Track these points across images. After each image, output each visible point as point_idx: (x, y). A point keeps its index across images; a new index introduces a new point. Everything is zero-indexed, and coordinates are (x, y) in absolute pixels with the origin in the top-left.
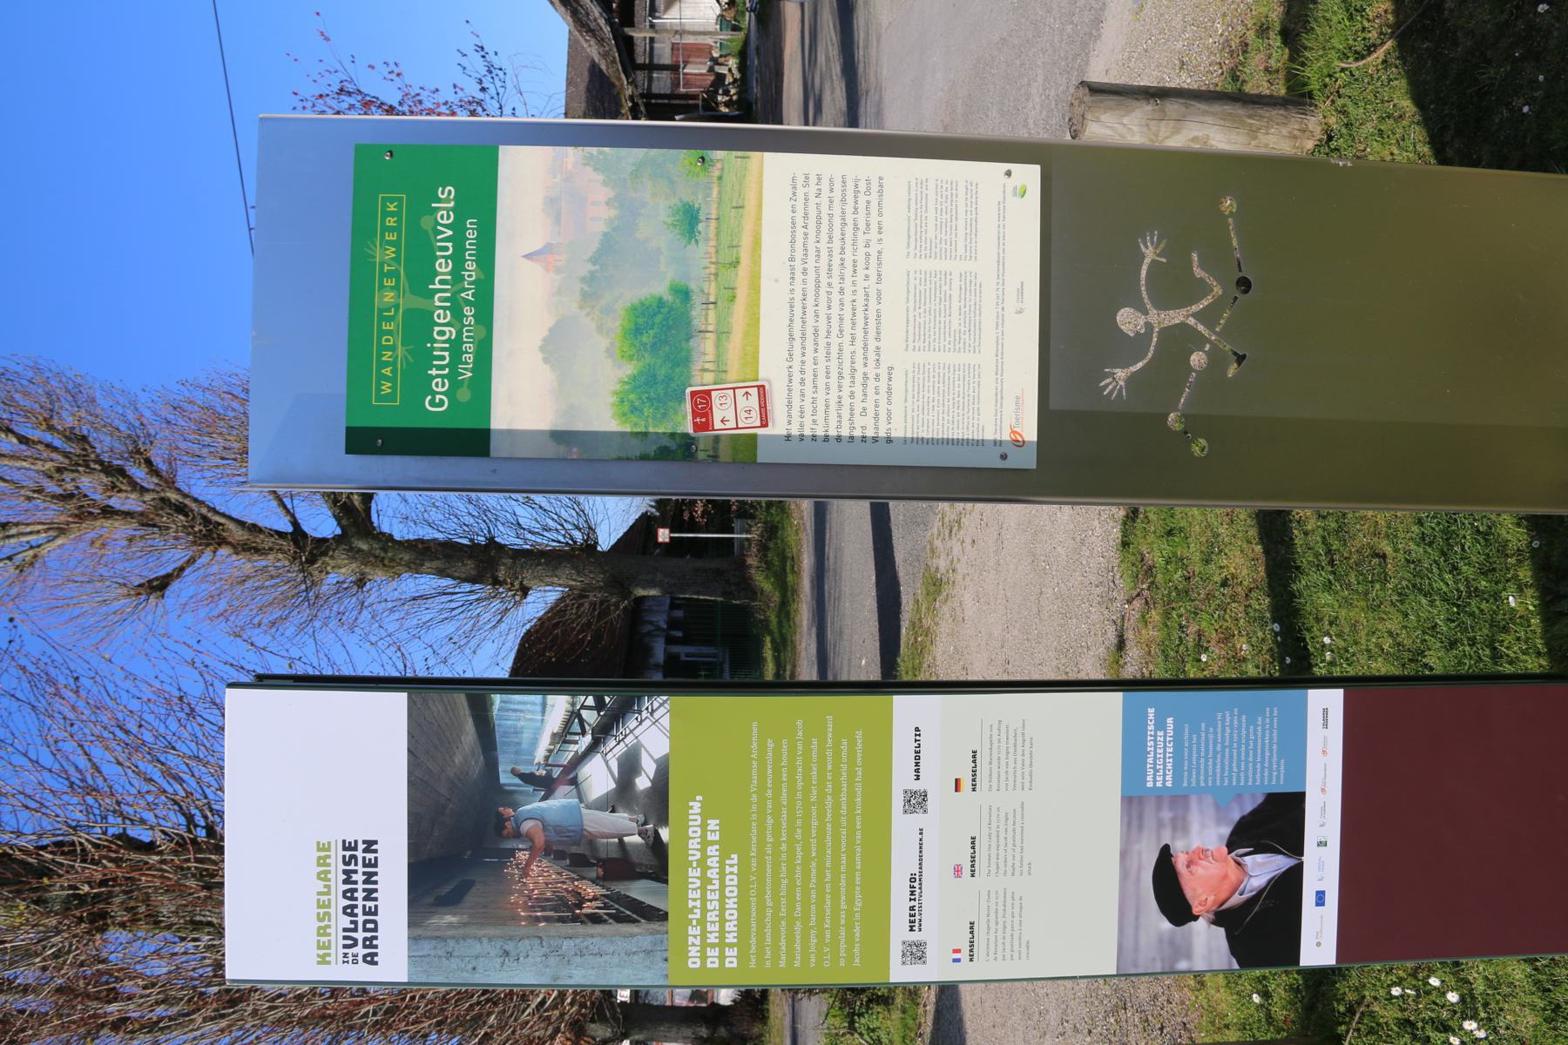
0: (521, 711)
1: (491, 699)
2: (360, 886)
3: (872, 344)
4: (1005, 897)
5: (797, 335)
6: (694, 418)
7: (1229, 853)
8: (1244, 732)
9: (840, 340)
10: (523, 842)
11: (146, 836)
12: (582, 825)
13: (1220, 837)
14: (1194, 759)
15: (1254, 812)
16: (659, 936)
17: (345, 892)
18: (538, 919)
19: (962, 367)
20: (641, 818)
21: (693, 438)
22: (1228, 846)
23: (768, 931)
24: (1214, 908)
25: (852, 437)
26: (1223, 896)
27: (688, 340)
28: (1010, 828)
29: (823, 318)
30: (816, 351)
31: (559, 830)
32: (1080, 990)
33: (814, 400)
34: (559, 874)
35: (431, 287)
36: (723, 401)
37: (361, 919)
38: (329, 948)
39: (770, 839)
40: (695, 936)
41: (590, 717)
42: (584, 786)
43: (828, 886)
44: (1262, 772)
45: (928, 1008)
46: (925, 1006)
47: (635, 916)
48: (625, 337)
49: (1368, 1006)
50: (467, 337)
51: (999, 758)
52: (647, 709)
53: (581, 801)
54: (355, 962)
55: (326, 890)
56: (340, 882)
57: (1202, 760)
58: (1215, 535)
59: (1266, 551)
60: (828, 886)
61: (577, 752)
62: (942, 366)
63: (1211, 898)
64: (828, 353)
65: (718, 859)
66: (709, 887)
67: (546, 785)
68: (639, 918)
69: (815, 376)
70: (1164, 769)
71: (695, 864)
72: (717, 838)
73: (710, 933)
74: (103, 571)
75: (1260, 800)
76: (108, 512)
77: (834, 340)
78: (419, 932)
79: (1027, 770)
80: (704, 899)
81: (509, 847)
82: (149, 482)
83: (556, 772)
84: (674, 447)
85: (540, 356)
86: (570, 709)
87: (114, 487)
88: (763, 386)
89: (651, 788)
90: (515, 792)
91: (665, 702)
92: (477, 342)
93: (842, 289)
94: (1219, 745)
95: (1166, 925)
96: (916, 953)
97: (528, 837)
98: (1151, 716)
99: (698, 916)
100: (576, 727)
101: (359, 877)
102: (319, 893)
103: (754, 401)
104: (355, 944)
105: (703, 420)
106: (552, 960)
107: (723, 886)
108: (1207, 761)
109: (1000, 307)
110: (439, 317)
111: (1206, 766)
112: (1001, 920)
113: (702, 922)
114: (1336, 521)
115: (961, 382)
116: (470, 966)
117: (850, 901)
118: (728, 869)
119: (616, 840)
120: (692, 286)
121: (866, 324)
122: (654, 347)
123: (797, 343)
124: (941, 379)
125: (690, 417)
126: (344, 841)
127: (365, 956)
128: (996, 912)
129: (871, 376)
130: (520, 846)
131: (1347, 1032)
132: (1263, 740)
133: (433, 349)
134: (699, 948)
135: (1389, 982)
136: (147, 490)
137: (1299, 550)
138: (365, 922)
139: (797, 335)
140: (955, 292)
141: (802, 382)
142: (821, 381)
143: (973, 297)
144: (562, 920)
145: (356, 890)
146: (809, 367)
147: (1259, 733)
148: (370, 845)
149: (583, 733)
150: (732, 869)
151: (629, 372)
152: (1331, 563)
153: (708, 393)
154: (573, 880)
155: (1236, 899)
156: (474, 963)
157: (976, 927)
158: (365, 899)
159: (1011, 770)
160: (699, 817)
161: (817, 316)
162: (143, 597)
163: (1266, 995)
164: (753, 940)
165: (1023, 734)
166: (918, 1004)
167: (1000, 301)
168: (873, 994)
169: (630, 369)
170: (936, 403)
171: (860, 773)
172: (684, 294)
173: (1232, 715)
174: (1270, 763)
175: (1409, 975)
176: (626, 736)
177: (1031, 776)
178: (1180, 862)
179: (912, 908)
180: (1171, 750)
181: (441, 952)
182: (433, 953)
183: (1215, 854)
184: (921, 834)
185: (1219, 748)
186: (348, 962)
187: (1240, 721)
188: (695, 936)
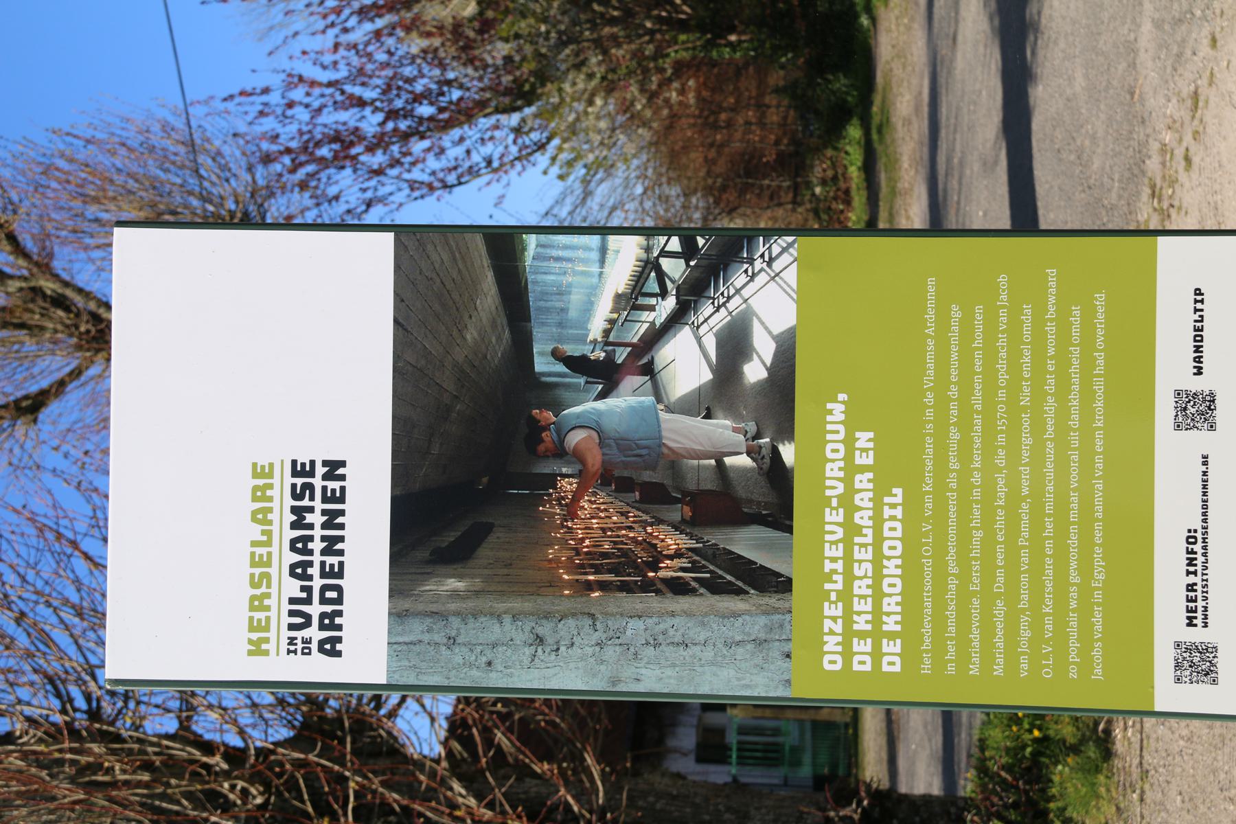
0: (569, 260)
1: (522, 241)
2: (318, 532)
10: (568, 463)
12: (660, 438)
16: (777, 617)
17: (293, 542)
18: (589, 586)
20: (752, 427)
23: (951, 613)
31: (624, 444)
34: (622, 514)
37: (317, 583)
38: (267, 629)
40: (834, 619)
41: (675, 269)
42: (664, 377)
43: (1049, 544)
47: (740, 584)
52: (762, 256)
53: (659, 400)
54: (307, 652)
56: (287, 525)
60: (1049, 544)
61: (653, 323)
65: (870, 494)
66: (857, 540)
71: (834, 502)
72: (870, 461)
73: (859, 613)
78: (406, 604)
80: (848, 559)
83: (621, 355)
86: (644, 256)
89: (767, 380)
91: (790, 245)
97: (577, 456)
99: (839, 586)
100: (652, 285)
101: (316, 519)
102: (255, 544)
104: (308, 624)
106: (611, 652)
107: (879, 539)
113: (846, 596)
116: (484, 659)
117: (1086, 570)
118: (887, 512)
126: (294, 462)
127: (322, 643)
130: (564, 470)
134: (839, 639)
138: (324, 589)
144: (626, 588)
145: (311, 539)
148: (334, 468)
149: (664, 294)
156: (489, 655)
158: (324, 552)
160: (841, 428)
164: (927, 629)
171: (1101, 362)
176: (729, 298)
179: (1191, 587)
182: (426, 638)
184: (1205, 463)
186: (295, 652)
188: (834, 619)
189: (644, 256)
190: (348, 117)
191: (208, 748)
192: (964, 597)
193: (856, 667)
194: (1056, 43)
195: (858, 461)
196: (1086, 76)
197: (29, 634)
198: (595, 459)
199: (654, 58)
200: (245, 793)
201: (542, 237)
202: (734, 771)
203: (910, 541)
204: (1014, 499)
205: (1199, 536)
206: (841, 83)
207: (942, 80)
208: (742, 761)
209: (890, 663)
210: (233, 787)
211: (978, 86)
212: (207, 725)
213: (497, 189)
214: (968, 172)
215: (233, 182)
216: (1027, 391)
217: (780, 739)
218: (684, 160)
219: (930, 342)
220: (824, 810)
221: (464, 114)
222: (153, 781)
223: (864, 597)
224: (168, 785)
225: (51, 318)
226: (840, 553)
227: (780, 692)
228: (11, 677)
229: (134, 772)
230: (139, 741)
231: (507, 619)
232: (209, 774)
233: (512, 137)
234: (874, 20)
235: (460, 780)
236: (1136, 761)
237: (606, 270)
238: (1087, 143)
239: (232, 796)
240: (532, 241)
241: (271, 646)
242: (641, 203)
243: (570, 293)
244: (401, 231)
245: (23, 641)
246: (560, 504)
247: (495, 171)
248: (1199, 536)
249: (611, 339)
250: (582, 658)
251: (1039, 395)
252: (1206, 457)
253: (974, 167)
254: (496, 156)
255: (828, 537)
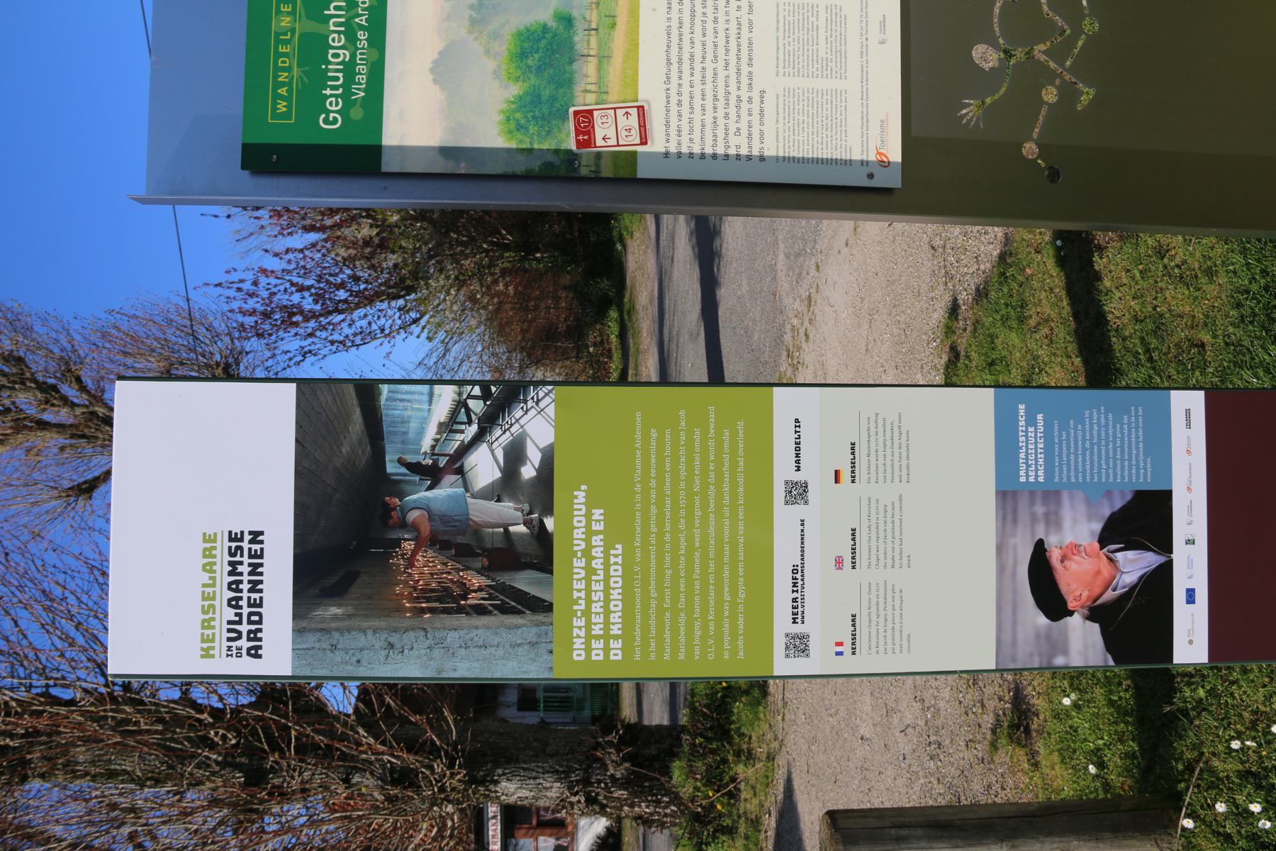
0: (408, 401)
1: (379, 389)
2: (246, 578)
3: (745, 69)
4: (885, 589)
5: (674, 60)
6: (577, 135)
7: (1101, 549)
8: (1111, 430)
9: (715, 66)
10: (408, 532)
11: (66, 695)
12: (468, 515)
13: (1092, 533)
14: (1064, 455)
15: (1123, 509)
16: (543, 628)
17: (230, 584)
18: (423, 611)
19: (829, 92)
20: (526, 507)
21: (576, 155)
22: (1099, 541)
23: (653, 622)
24: (1088, 603)
25: (727, 156)
26: (1097, 591)
27: (571, 63)
28: (889, 520)
29: (698, 46)
30: (692, 75)
31: (445, 519)
32: (914, 794)
33: (691, 121)
34: (444, 564)
35: (326, 12)
36: (604, 120)
37: (246, 611)
38: (213, 641)
39: (654, 529)
40: (580, 628)
41: (477, 406)
42: (470, 475)
43: (711, 577)
44: (1130, 470)
45: (769, 833)
46: (766, 832)
47: (520, 607)
48: (511, 60)
49: (1207, 762)
50: (360, 59)
51: (877, 451)
52: (533, 398)
53: (467, 490)
54: (239, 655)
55: (211, 582)
56: (225, 573)
57: (1072, 457)
58: (1036, 358)
59: (1086, 362)
60: (711, 577)
61: (463, 441)
62: (811, 91)
63: (1085, 594)
64: (704, 77)
65: (602, 549)
66: (594, 578)
67: (433, 474)
68: (524, 610)
69: (692, 98)
70: (1036, 464)
71: (579, 554)
72: (601, 528)
73: (595, 624)
74: (36, 475)
75: (1129, 497)
76: (43, 425)
77: (709, 66)
78: (304, 624)
79: (904, 462)
80: (588, 590)
81: (395, 537)
82: (81, 399)
83: (443, 462)
84: (557, 163)
85: (431, 77)
86: (457, 398)
87: (47, 402)
88: (643, 107)
89: (536, 478)
90: (401, 481)
91: (550, 391)
92: (369, 65)
93: (716, 18)
94: (1088, 442)
95: (1042, 620)
96: (799, 645)
97: (414, 527)
98: (1022, 412)
99: (583, 607)
100: (462, 417)
101: (244, 569)
102: (204, 585)
103: (634, 121)
104: (239, 637)
105: (586, 137)
106: (437, 653)
107: (607, 577)
108: (1076, 457)
109: (864, 38)
110: (333, 40)
111: (1076, 462)
112: (882, 613)
113: (587, 613)
114: (1154, 323)
115: (829, 106)
116: (355, 659)
117: (734, 593)
118: (612, 560)
119: (502, 530)
120: (575, 13)
121: (739, 50)
122: (539, 70)
123: (674, 68)
124: (810, 103)
125: (573, 134)
126: (230, 532)
127: (249, 649)
128: (877, 604)
129: (745, 98)
130: (406, 536)
131: (1188, 788)
132: (1130, 438)
133: (327, 70)
134: (583, 640)
135: (1227, 737)
136: (78, 405)
137: (1118, 355)
138: (250, 614)
139: (674, 60)
140: (822, 23)
141: (679, 103)
142: (698, 102)
143: (838, 28)
144: (446, 611)
145: (241, 582)
146: (686, 90)
147: (1126, 431)
148: (256, 536)
149: (470, 422)
150: (616, 560)
151: (516, 93)
152: (1151, 359)
153: (590, 112)
154: (458, 570)
155: (1109, 595)
156: (358, 656)
157: (858, 618)
158: (250, 591)
159: (888, 463)
160: (583, 507)
161: (693, 43)
162: (72, 499)
163: (1101, 765)
164: (638, 632)
165: (899, 427)
166: (760, 831)
167: (864, 32)
168: (718, 825)
169: (516, 90)
170: (806, 125)
171: (741, 463)
172: (567, 21)
173: (1099, 413)
174: (1138, 461)
175: (1247, 728)
176: (512, 425)
177: (908, 468)
178: (1055, 556)
179: (795, 600)
180: (1042, 446)
181: (325, 645)
182: (317, 645)
183: (1087, 548)
184: (802, 525)
185: (1088, 445)
186: (232, 655)
187: (1106, 419)
188: (580, 628)
189: (457, 398)
190: (296, 298)
191: (199, 708)
192: (660, 610)
193: (594, 658)
194: (731, 264)
195: (594, 528)
196: (749, 284)
197: (84, 636)
198: (426, 529)
199: (489, 267)
200: (224, 737)
201: (392, 386)
202: (541, 715)
203: (627, 576)
204: (690, 549)
205: (799, 568)
206: (605, 284)
207: (665, 284)
208: (546, 709)
209: (615, 655)
210: (216, 734)
211: (687, 288)
212: (198, 694)
213: (387, 347)
214: (682, 340)
215: (219, 343)
216: (697, 482)
217: (570, 694)
218: (508, 330)
219: (638, 452)
220: (595, 738)
221: (368, 299)
222: (165, 730)
223: (599, 614)
224: (175, 732)
225: (101, 431)
226: (583, 587)
227: (546, 675)
228: (73, 664)
229: (152, 724)
230: (156, 704)
231: (370, 633)
232: (200, 725)
233: (398, 315)
234: (624, 246)
235: (363, 727)
236: (781, 697)
237: (433, 407)
238: (750, 324)
239: (216, 739)
240: (385, 388)
241: (216, 652)
242: (481, 357)
243: (409, 422)
244: (300, 382)
245: (80, 640)
246: (403, 558)
247: (386, 336)
248: (799, 568)
249: (436, 451)
250: (419, 657)
251: (705, 485)
252: (802, 521)
253: (684, 338)
254: (387, 326)
255: (575, 576)
